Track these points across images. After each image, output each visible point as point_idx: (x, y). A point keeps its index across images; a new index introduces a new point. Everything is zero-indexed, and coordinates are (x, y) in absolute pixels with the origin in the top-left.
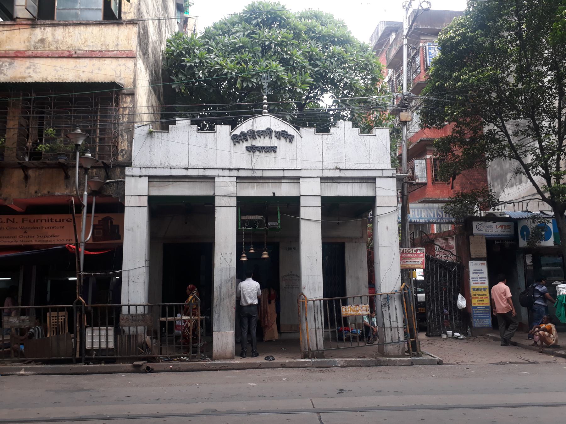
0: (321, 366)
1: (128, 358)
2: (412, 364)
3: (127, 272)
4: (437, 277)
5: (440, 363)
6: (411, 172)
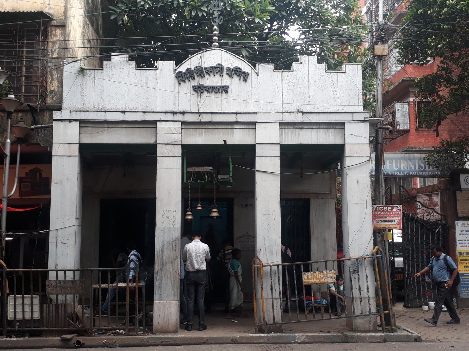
0: (278, 341)
1: (55, 330)
2: (385, 341)
3: (55, 232)
4: (417, 240)
5: (418, 340)
6: (391, 117)
